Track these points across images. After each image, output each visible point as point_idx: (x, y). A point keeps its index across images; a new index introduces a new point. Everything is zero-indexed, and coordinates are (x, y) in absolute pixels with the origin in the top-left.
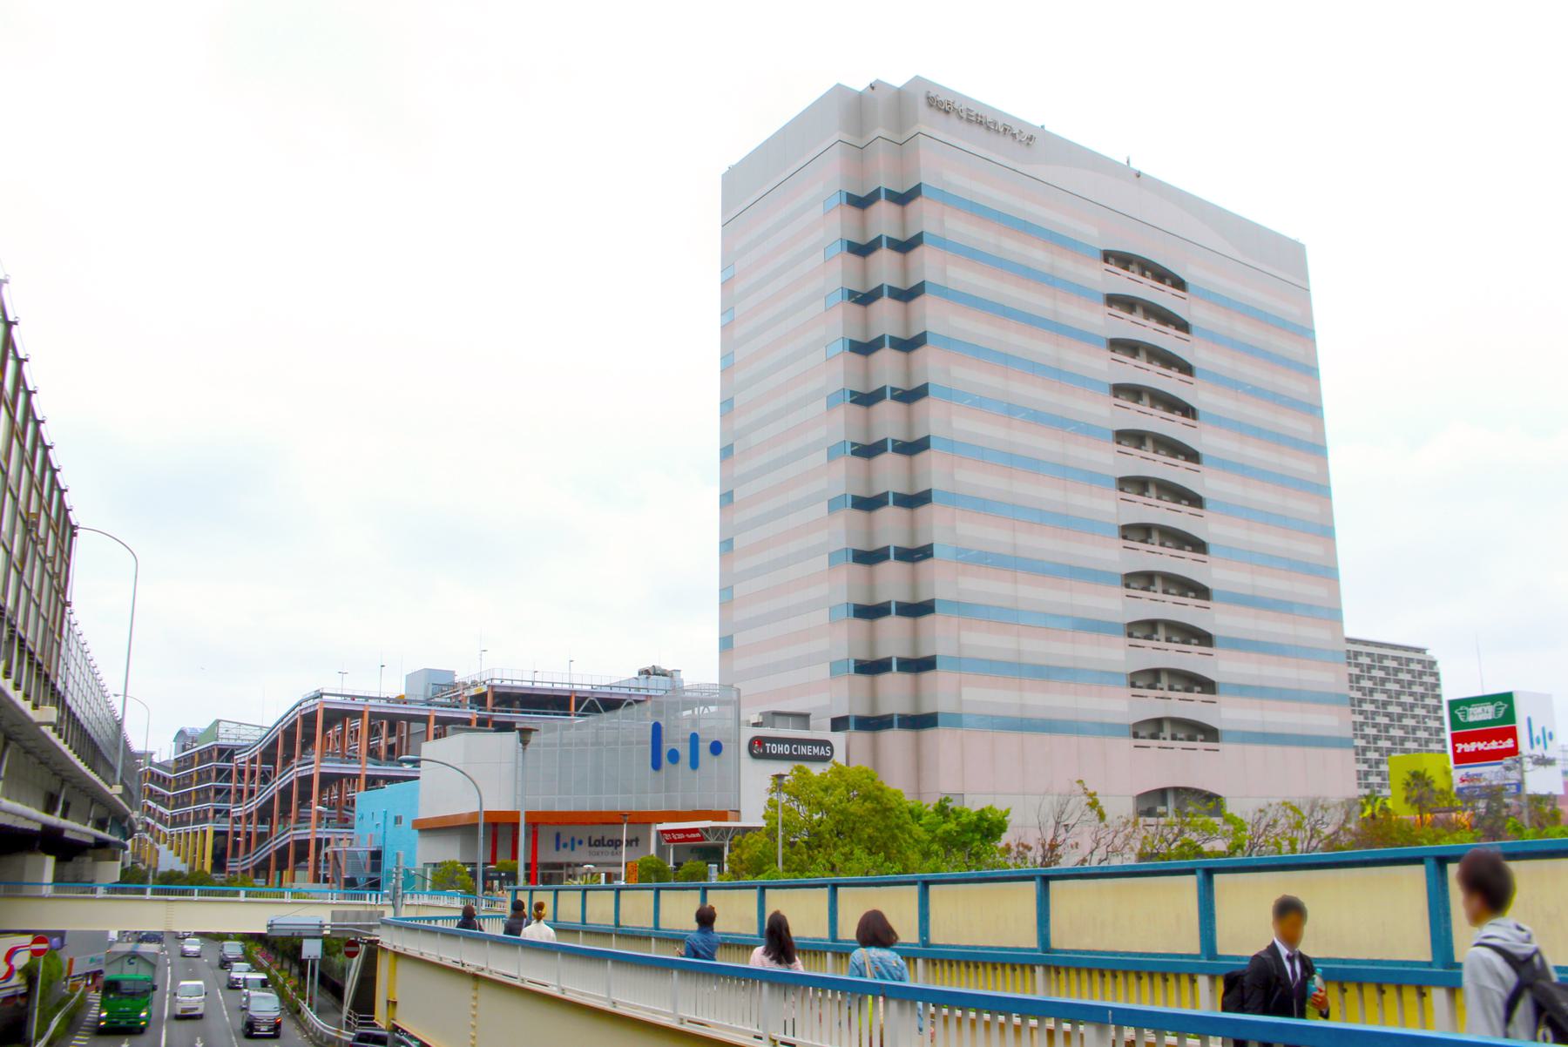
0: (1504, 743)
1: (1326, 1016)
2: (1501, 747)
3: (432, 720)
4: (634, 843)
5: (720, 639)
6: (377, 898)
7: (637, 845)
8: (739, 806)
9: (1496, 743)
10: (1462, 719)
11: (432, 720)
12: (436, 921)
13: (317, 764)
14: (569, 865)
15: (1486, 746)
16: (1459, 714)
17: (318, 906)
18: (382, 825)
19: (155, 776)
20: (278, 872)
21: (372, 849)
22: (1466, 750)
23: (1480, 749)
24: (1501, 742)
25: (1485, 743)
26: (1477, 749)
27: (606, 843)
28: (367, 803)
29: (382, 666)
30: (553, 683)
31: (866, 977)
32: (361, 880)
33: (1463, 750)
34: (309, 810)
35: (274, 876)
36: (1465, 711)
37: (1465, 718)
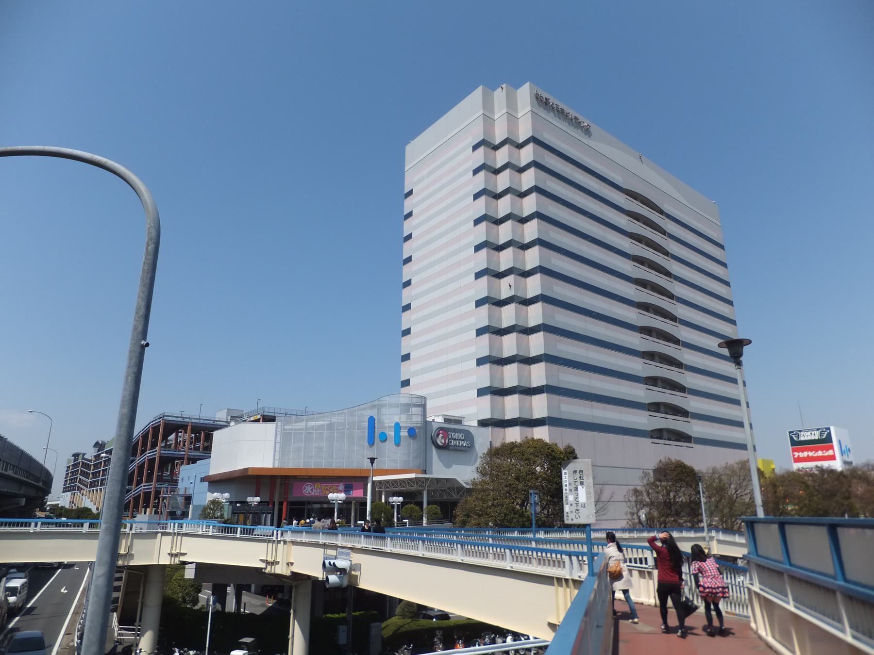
0: (827, 452)
2: (824, 454)
5: (211, 451)
6: (174, 527)
8: (426, 468)
9: (822, 452)
10: (795, 439)
12: (266, 530)
15: (814, 454)
16: (793, 436)
17: (427, 461)
18: (193, 483)
20: (143, 509)
22: (800, 456)
23: (810, 456)
24: (824, 452)
25: (814, 452)
26: (808, 456)
30: (274, 413)
31: (118, 598)
32: (179, 513)
33: (799, 456)
34: (209, 455)
35: (141, 510)
36: (798, 434)
37: (798, 438)
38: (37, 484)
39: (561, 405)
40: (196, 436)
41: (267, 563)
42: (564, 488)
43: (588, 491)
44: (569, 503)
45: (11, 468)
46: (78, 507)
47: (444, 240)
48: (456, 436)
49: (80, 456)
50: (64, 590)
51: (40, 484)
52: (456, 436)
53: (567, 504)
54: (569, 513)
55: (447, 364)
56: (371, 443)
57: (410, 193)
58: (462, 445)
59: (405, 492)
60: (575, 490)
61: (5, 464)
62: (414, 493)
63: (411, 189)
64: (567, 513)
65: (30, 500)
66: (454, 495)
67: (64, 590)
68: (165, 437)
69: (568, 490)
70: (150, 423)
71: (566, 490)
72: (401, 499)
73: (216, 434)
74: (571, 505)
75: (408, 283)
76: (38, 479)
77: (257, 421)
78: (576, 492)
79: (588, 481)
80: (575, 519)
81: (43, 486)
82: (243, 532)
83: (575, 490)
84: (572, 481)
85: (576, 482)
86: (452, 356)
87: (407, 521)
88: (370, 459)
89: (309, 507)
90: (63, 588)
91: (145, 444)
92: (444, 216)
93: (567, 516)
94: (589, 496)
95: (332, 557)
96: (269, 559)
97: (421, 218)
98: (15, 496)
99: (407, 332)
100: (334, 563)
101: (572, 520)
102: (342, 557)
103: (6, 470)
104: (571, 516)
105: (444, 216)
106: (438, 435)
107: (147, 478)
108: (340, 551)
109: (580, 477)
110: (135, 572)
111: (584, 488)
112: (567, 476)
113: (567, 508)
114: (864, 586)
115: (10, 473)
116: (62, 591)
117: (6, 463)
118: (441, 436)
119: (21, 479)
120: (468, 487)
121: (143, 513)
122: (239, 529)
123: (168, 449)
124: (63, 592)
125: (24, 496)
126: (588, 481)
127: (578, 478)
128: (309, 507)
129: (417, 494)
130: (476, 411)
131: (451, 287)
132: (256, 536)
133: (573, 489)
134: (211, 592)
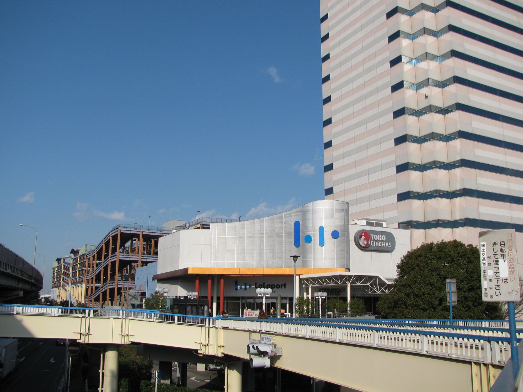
1: (129, 250)
3: (141, 236)
4: (283, 287)
7: (285, 288)
11: (141, 236)
13: (119, 256)
14: (243, 298)
19: (65, 273)
21: (141, 291)
27: (265, 286)
28: (140, 272)
29: (150, 217)
38: (30, 281)
39: (478, 178)
40: (147, 243)
41: (202, 345)
42: (482, 262)
43: (511, 265)
44: (488, 278)
45: (9, 268)
46: (63, 300)
47: (360, 58)
48: (377, 237)
49: (62, 261)
50: (52, 360)
51: (33, 281)
52: (377, 237)
53: (485, 279)
54: (488, 289)
55: (368, 172)
56: (297, 244)
57: (326, 17)
58: (384, 246)
59: (330, 288)
60: (495, 264)
61: (4, 264)
62: (338, 289)
63: (327, 13)
64: (486, 289)
65: (26, 292)
66: (377, 292)
67: (52, 360)
68: (122, 245)
69: (486, 264)
70: (110, 233)
71: (484, 264)
72: (325, 294)
73: (160, 240)
74: (490, 280)
75: (328, 100)
76: (31, 277)
77: (199, 228)
78: (497, 266)
79: (510, 254)
80: (494, 296)
81: (34, 282)
82: (180, 319)
83: (495, 264)
84: (492, 254)
85: (496, 255)
86: (372, 165)
87: (332, 313)
88: (294, 257)
89: (244, 301)
90: (51, 358)
91: (107, 250)
92: (359, 36)
93: (486, 293)
94: (512, 270)
95: (256, 342)
96: (203, 342)
97: (337, 40)
98: (16, 289)
99: (329, 144)
100: (257, 347)
101: (491, 297)
102: (265, 342)
103: (6, 269)
104: (490, 293)
105: (359, 36)
106: (361, 237)
107: (110, 277)
108: (263, 336)
109: (501, 249)
110: (96, 348)
111: (506, 261)
112: (485, 248)
113: (485, 284)
114: (489, 378)
115: (9, 271)
116: (51, 361)
117: (5, 264)
118: (363, 237)
119: (20, 277)
120: (390, 283)
121: (110, 305)
122: (176, 317)
123: (126, 254)
124: (51, 362)
125: (21, 289)
126: (510, 254)
127: (499, 250)
128: (244, 301)
129: (342, 290)
130: (333, 152)
131: (370, 101)
132: (191, 324)
133: (493, 263)
134: (172, 368)
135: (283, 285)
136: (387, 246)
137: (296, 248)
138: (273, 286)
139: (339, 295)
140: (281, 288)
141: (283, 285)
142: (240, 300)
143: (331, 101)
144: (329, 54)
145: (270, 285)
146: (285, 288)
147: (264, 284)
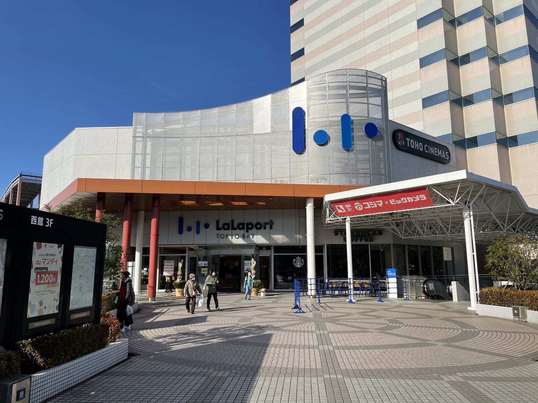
4: (268, 227)
7: (271, 228)
27: (235, 226)
135: (267, 224)
136: (444, 157)
137: (210, 226)
138: (250, 226)
139: (371, 240)
140: (265, 228)
141: (267, 224)
142: (185, 253)
143: (304, 54)
144: (303, 20)
145: (243, 224)
146: (271, 228)
147: (233, 221)
